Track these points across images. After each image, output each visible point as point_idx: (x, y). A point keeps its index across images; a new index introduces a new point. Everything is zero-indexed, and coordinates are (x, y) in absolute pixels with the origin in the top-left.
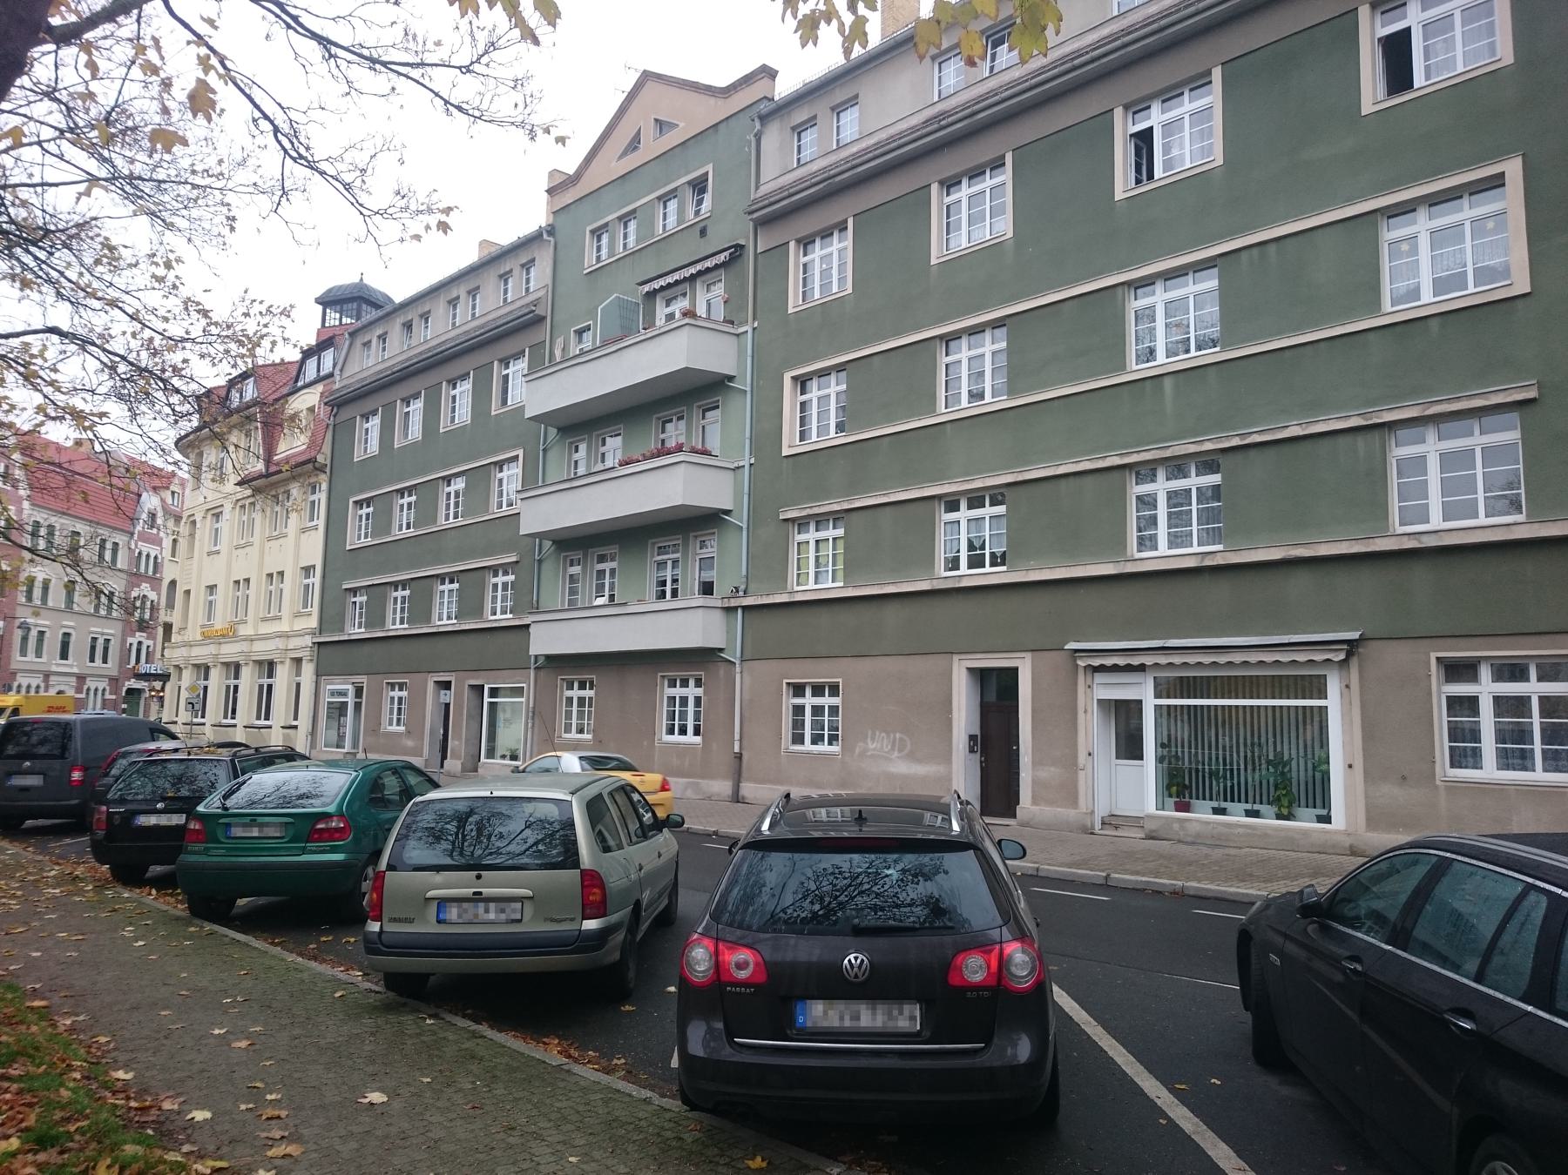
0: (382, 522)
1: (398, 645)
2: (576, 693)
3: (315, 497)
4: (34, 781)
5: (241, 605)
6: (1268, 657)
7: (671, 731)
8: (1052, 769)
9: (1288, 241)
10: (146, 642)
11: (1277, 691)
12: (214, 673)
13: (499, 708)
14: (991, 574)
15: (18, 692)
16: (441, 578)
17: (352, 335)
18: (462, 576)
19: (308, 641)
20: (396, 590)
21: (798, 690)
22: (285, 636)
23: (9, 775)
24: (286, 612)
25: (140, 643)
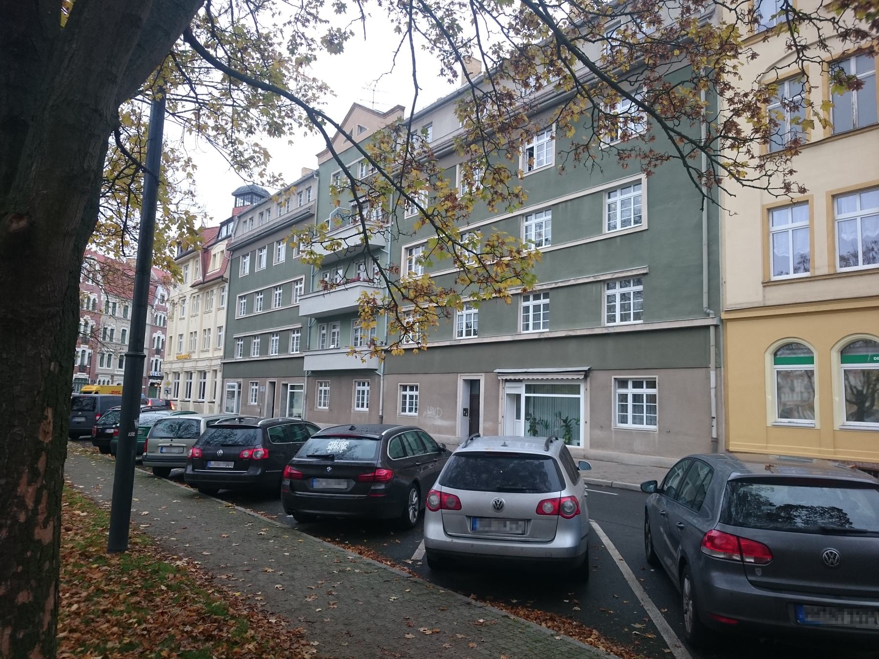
0: (250, 307)
1: (255, 364)
2: (323, 388)
3: (223, 294)
4: (83, 419)
5: (193, 343)
6: (560, 377)
7: (358, 406)
9: (584, 198)
10: (160, 360)
12: (194, 376)
13: (295, 394)
14: (473, 339)
15: (99, 384)
16: (272, 334)
17: (239, 217)
18: (281, 333)
19: (219, 362)
20: (294, 333)
22: (210, 359)
23: (74, 417)
24: (211, 349)
25: (157, 360)
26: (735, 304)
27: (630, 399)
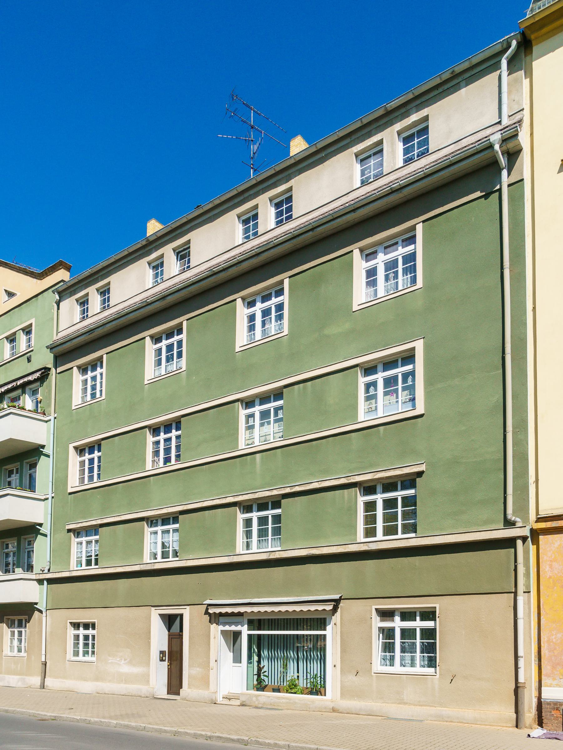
8: (198, 669)
11: (276, 627)
21: (76, 626)
26: (552, 509)
27: (81, 638)
